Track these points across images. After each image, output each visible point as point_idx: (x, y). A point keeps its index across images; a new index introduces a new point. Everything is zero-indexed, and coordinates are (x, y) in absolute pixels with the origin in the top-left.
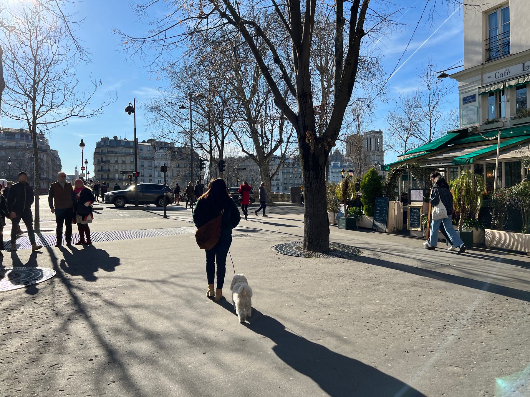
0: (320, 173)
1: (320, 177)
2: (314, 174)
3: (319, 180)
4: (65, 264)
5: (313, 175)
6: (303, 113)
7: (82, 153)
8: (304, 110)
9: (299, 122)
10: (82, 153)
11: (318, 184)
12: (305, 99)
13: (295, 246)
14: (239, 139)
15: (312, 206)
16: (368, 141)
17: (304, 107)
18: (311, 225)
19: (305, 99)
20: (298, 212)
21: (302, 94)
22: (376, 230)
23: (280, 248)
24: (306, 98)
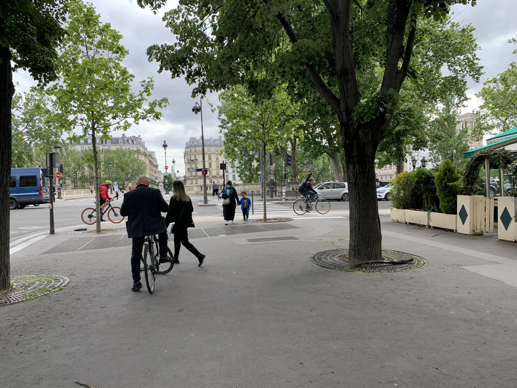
0: (368, 166)
1: (367, 170)
2: (359, 167)
3: (366, 174)
4: (142, 247)
5: (358, 169)
6: (345, 94)
7: (165, 153)
8: (345, 90)
9: (341, 105)
10: (165, 153)
11: (365, 179)
12: (346, 77)
13: (337, 254)
14: (95, 149)
15: (358, 206)
16: (463, 125)
17: (345, 87)
18: (357, 229)
19: (346, 77)
20: (344, 209)
21: (342, 72)
22: (454, 231)
23: (480, 60)
24: (347, 77)
